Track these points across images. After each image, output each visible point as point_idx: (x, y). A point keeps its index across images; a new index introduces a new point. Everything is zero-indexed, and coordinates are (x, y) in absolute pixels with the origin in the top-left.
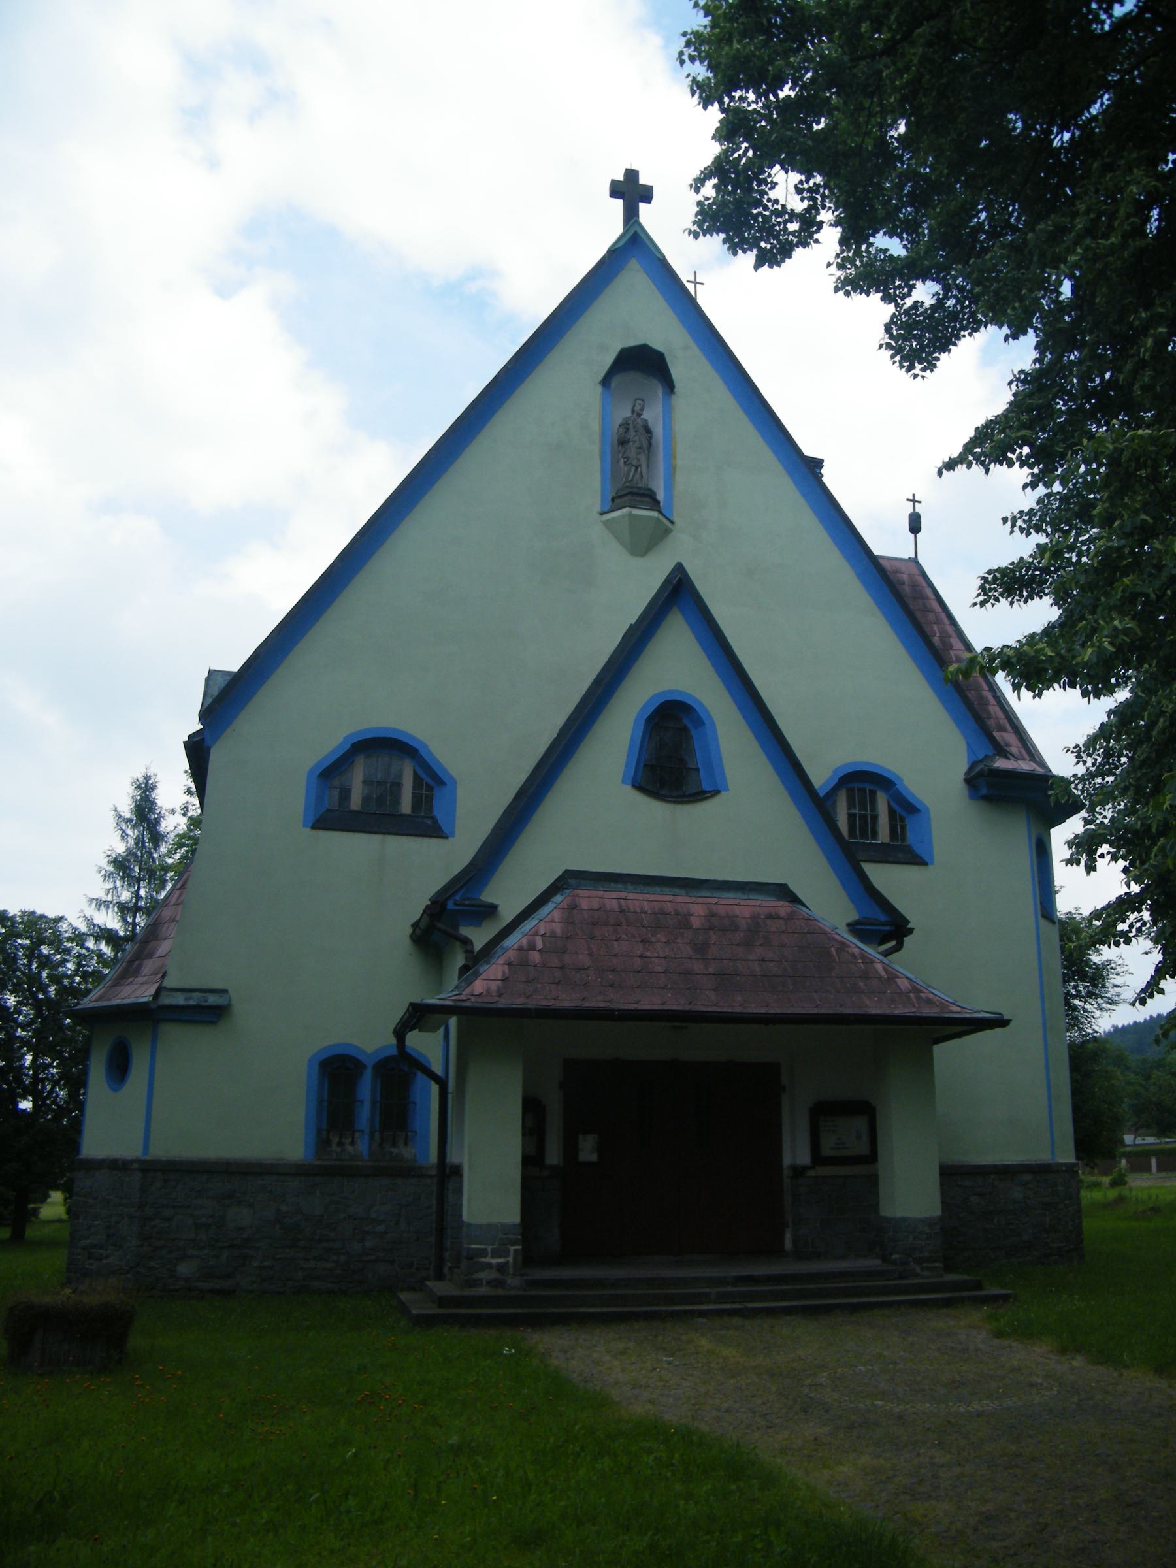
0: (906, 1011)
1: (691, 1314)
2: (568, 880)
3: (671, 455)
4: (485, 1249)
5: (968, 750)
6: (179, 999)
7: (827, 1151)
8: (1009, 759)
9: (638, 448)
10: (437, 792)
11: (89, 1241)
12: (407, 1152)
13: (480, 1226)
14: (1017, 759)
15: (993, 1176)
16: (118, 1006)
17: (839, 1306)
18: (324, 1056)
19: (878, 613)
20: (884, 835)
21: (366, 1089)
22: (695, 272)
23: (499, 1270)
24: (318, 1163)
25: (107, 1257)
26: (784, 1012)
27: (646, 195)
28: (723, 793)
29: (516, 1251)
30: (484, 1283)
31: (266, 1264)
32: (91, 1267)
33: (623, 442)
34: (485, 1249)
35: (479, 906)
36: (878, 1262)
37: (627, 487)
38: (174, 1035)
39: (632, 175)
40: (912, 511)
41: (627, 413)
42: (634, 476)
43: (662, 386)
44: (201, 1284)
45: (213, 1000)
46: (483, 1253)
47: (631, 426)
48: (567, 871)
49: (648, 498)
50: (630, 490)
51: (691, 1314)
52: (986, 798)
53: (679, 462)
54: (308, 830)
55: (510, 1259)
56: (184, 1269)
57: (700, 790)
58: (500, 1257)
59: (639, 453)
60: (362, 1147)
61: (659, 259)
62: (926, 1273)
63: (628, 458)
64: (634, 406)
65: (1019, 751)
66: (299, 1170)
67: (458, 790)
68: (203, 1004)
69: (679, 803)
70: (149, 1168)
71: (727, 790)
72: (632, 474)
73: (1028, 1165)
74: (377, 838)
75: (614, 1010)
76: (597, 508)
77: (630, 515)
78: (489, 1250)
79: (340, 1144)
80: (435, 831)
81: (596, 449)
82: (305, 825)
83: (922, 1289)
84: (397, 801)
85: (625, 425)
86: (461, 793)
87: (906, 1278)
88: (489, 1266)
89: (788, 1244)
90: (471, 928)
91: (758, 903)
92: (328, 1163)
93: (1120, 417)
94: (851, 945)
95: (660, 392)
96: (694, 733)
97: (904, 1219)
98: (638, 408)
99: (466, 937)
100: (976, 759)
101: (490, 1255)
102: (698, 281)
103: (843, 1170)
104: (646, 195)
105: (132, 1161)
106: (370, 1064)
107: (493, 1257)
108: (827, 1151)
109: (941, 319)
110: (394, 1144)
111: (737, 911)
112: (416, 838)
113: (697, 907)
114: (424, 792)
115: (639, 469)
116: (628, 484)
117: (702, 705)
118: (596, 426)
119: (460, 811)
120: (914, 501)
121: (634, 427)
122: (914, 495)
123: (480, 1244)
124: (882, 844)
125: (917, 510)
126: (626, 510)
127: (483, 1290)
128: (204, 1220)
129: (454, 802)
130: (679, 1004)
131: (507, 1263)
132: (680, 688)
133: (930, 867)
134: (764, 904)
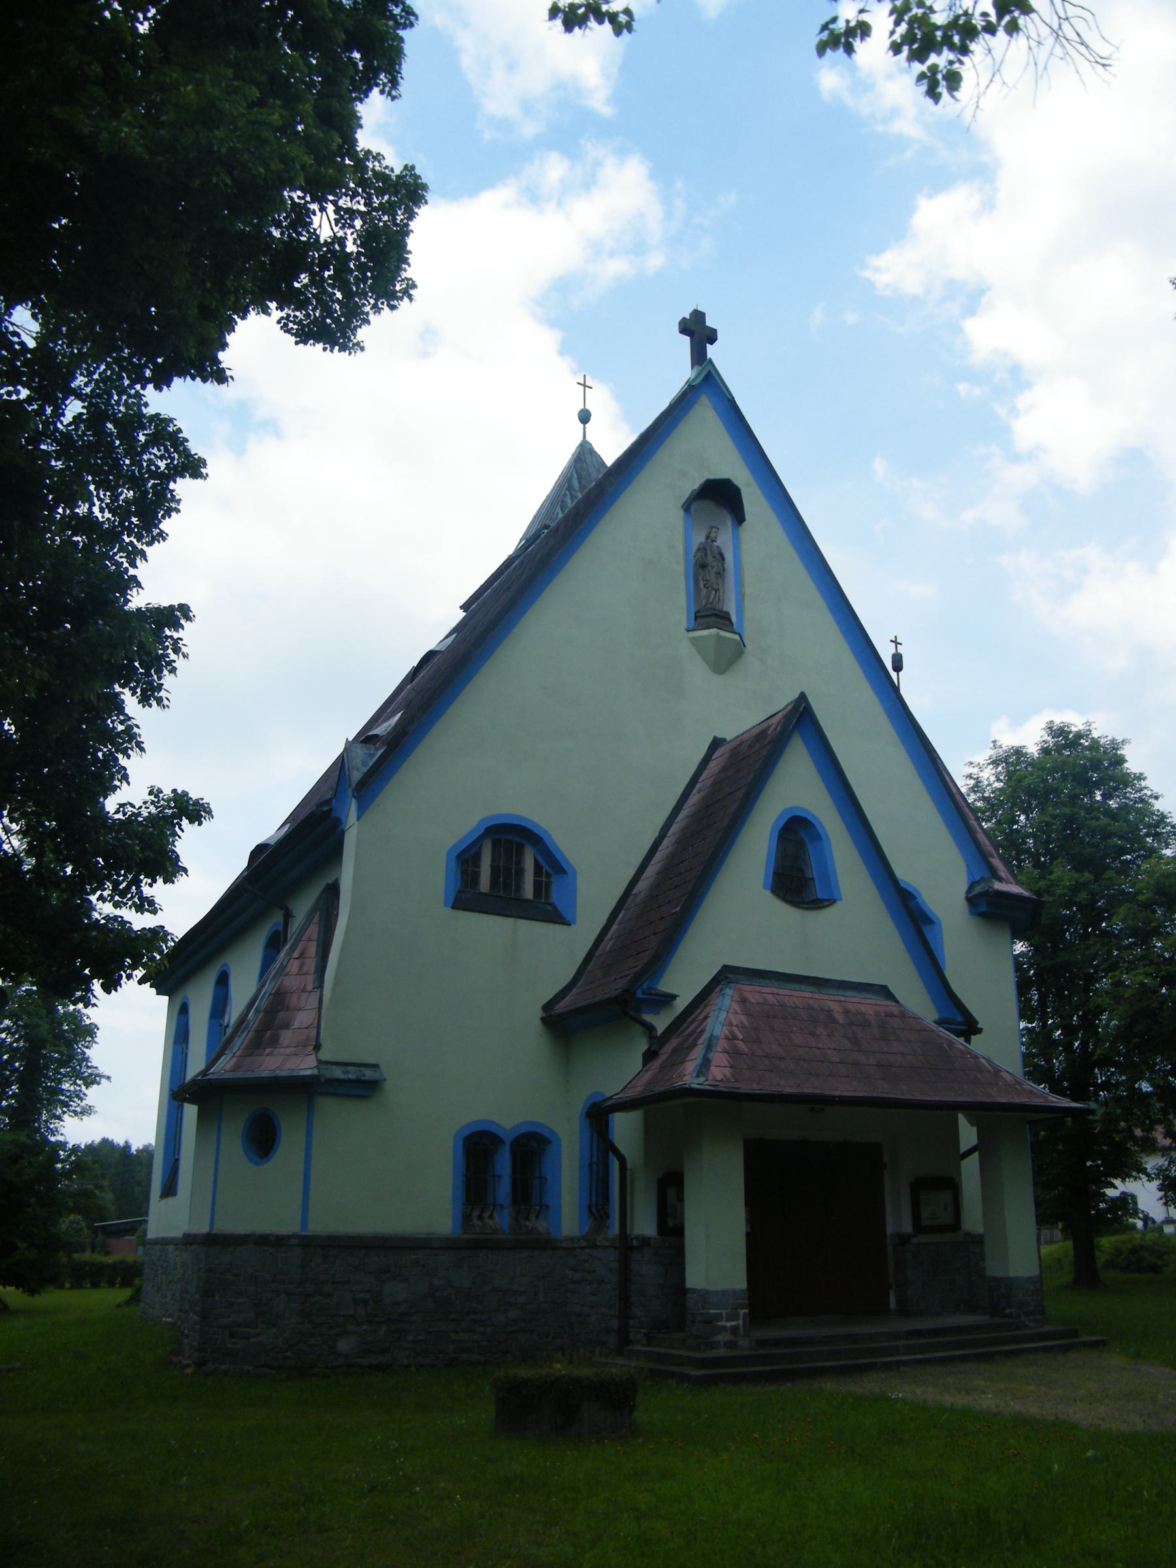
0: (1024, 1101)
2: (727, 975)
3: (740, 584)
4: (721, 1314)
5: (968, 873)
6: (338, 1073)
7: (925, 1222)
8: (1002, 882)
9: (716, 573)
10: (555, 879)
11: (230, 1320)
12: (541, 1225)
13: (717, 1292)
14: (1007, 883)
16: (247, 1078)
18: (467, 1132)
19: (901, 746)
21: (503, 1164)
22: (585, 376)
23: (732, 1333)
24: (466, 1236)
25: (257, 1335)
26: (933, 1099)
27: (712, 337)
29: (744, 1314)
30: (722, 1344)
31: (421, 1338)
32: (235, 1346)
33: (703, 566)
34: (721, 1314)
35: (656, 995)
36: (988, 1317)
37: (708, 609)
38: (329, 1109)
39: (698, 317)
40: (894, 651)
41: (703, 539)
42: (714, 599)
43: (732, 521)
44: (359, 1360)
45: (369, 1074)
46: (719, 1317)
47: (709, 552)
48: (725, 967)
49: (722, 619)
50: (714, 612)
52: (983, 915)
53: (748, 590)
54: (449, 910)
55: (741, 1322)
56: (345, 1345)
57: (815, 897)
58: (732, 1321)
59: (717, 578)
60: (501, 1221)
61: (729, 400)
62: (1033, 1325)
63: (708, 581)
64: (710, 533)
65: (1006, 876)
66: (450, 1245)
67: (578, 881)
68: (362, 1078)
69: (807, 909)
70: (309, 1244)
71: (841, 899)
72: (712, 596)
74: (511, 920)
75: (835, 1097)
76: (684, 625)
77: (718, 636)
78: (724, 1315)
79: (480, 1218)
80: (557, 917)
81: (681, 568)
82: (446, 905)
83: (1042, 1337)
84: (519, 887)
85: (703, 549)
86: (581, 884)
88: (724, 1329)
89: (893, 1304)
91: (874, 1002)
92: (475, 1237)
94: (956, 1042)
95: (729, 523)
96: (810, 847)
97: (1016, 1279)
98: (713, 535)
99: (651, 1023)
100: (973, 880)
101: (725, 1319)
102: (587, 384)
103: (938, 1238)
104: (712, 337)
105: (289, 1237)
106: (508, 1141)
107: (728, 1320)
108: (925, 1222)
110: (527, 1218)
111: (863, 1008)
112: (543, 924)
113: (831, 1001)
114: (544, 879)
115: (718, 593)
116: (709, 606)
117: (819, 822)
118: (680, 548)
119: (580, 900)
120: (896, 642)
121: (712, 553)
122: (896, 637)
125: (899, 651)
126: (714, 631)
127: (722, 1352)
128: (362, 1295)
129: (574, 891)
130: (866, 1091)
132: (802, 806)
134: (878, 1002)
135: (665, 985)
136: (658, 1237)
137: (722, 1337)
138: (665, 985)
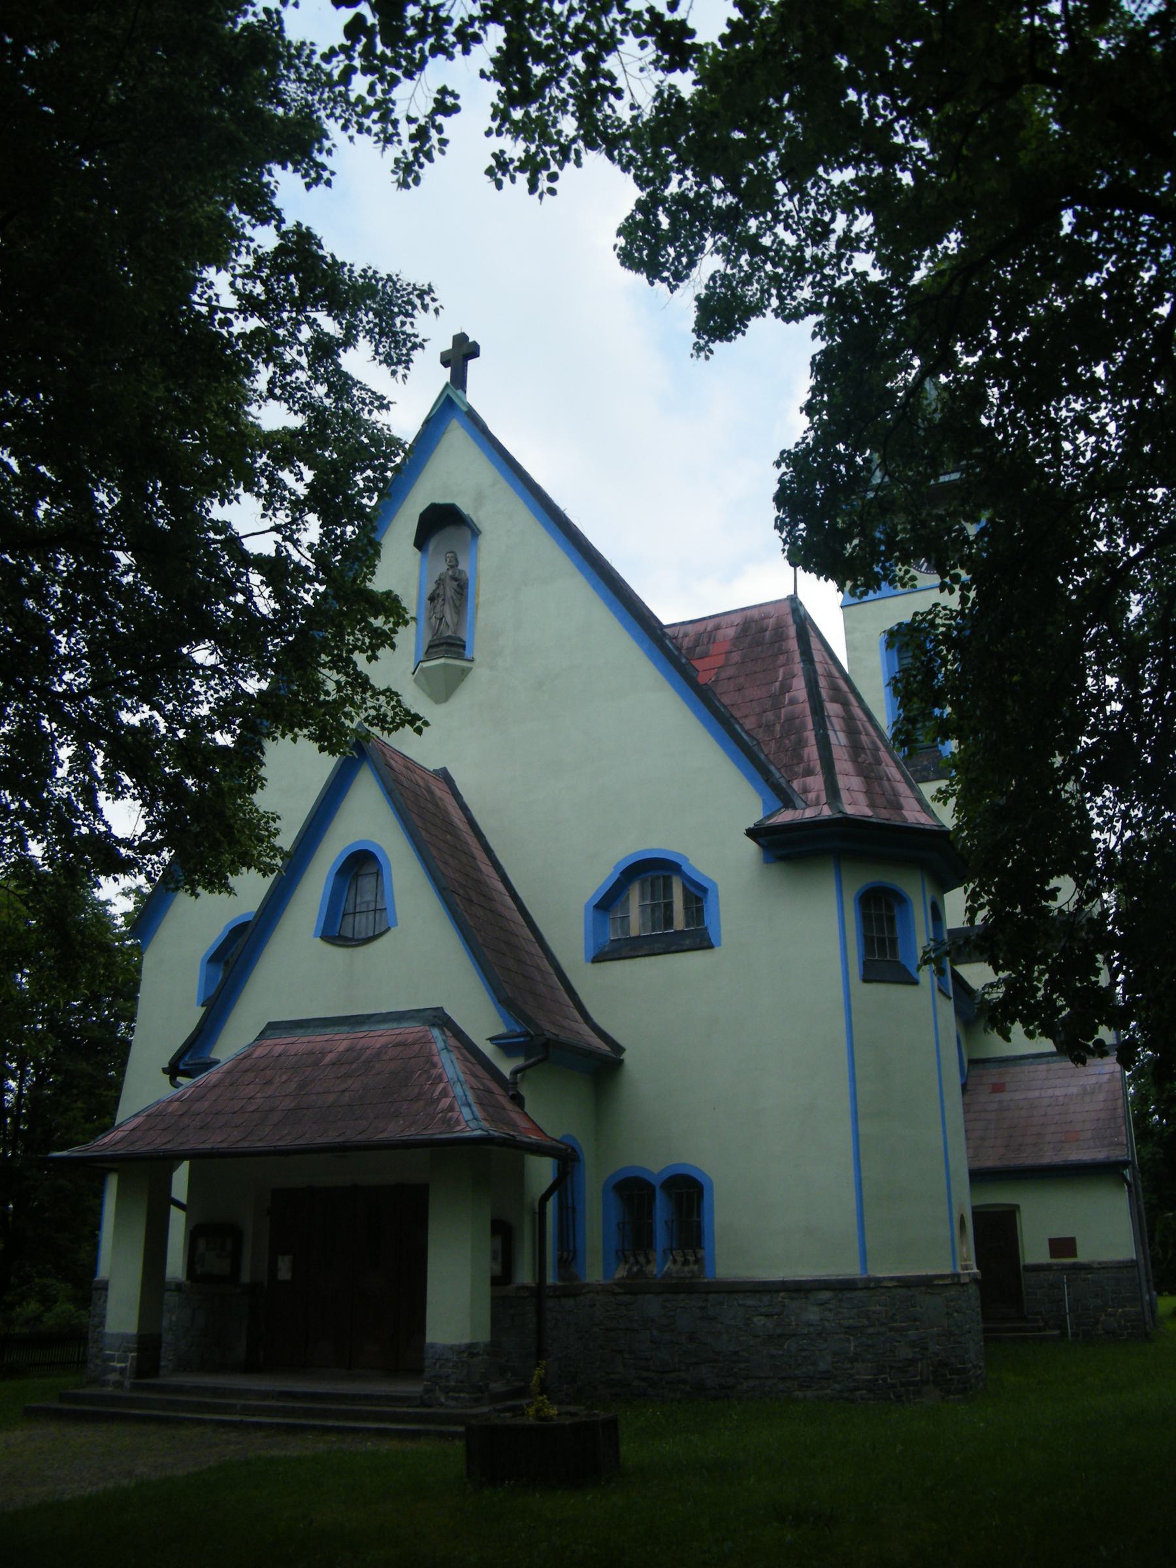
1: (304, 1429)
2: (273, 1028)
15: (782, 1294)
17: (314, 1427)
20: (679, 922)
21: (662, 1211)
28: (392, 929)
29: (132, 1357)
51: (304, 1429)
54: (590, 964)
55: (128, 1364)
62: (453, 1403)
73: (825, 1280)
87: (430, 1406)
88: (114, 1369)
90: (609, 1056)
93: (1088, 375)
107: (119, 1362)
109: (349, 500)
123: (111, 1350)
124: (676, 932)
126: (442, 661)
127: (109, 1389)
131: (126, 1367)
133: (716, 949)
135: (215, 1055)
136: (188, 1282)
137: (113, 1377)
138: (215, 1055)
